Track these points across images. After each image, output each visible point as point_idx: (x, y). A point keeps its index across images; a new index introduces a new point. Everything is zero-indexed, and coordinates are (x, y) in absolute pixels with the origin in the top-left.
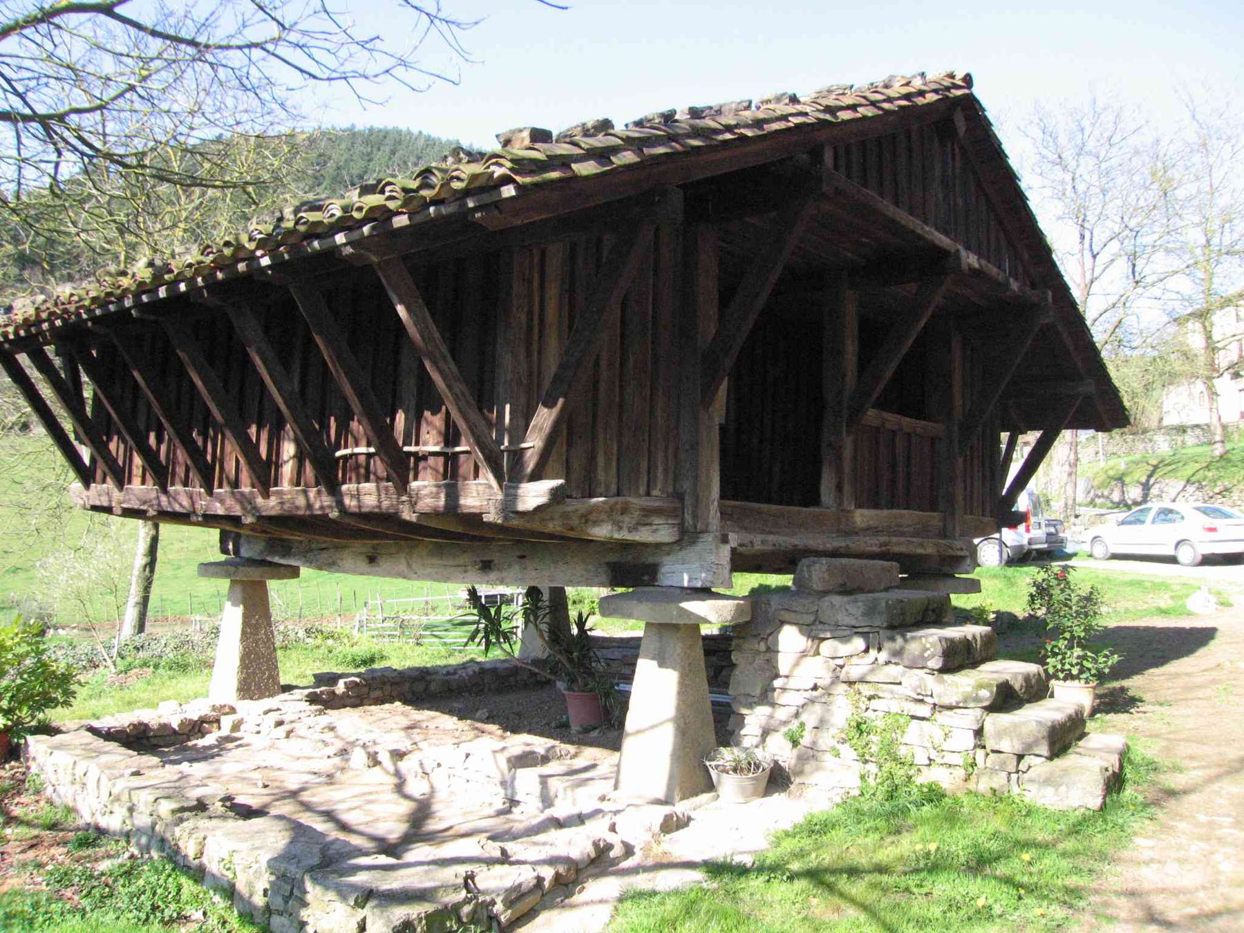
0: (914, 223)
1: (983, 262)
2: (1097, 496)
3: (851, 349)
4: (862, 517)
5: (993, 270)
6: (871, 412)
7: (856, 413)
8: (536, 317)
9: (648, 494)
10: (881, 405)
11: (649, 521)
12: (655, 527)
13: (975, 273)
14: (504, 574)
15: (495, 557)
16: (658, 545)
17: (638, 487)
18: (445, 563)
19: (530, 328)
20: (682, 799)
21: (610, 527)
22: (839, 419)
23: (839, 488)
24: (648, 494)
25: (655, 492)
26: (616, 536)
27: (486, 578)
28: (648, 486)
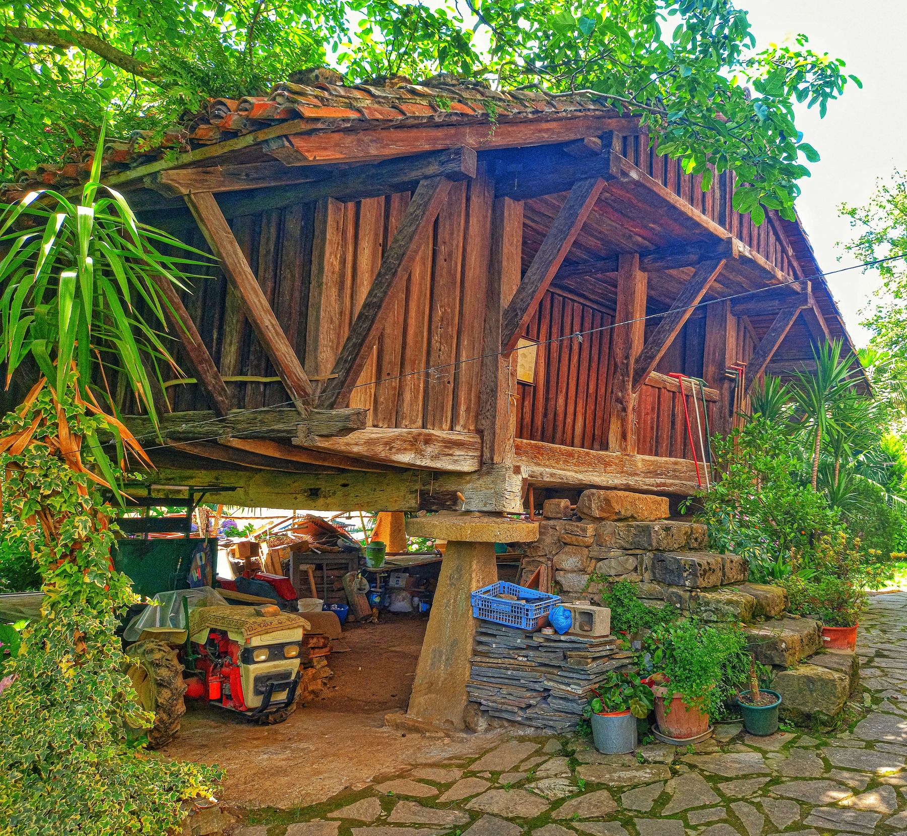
0: (695, 213)
1: (754, 253)
2: (280, 95)
3: (639, 320)
4: (641, 460)
5: (761, 260)
6: (653, 374)
7: (640, 375)
8: (349, 265)
9: (451, 429)
10: (658, 369)
11: (451, 452)
12: (456, 458)
13: (743, 259)
14: (329, 500)
15: (322, 485)
16: (460, 474)
17: (441, 423)
18: (276, 491)
19: (342, 275)
20: (42, 303)
21: (413, 456)
22: (626, 379)
23: (624, 436)
24: (451, 429)
25: (458, 428)
26: (418, 463)
27: (314, 505)
28: (452, 422)
